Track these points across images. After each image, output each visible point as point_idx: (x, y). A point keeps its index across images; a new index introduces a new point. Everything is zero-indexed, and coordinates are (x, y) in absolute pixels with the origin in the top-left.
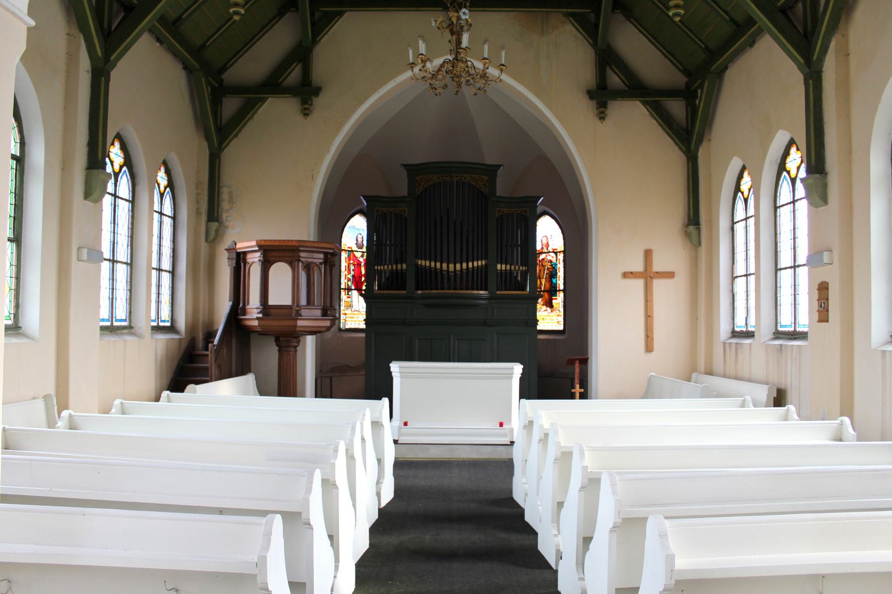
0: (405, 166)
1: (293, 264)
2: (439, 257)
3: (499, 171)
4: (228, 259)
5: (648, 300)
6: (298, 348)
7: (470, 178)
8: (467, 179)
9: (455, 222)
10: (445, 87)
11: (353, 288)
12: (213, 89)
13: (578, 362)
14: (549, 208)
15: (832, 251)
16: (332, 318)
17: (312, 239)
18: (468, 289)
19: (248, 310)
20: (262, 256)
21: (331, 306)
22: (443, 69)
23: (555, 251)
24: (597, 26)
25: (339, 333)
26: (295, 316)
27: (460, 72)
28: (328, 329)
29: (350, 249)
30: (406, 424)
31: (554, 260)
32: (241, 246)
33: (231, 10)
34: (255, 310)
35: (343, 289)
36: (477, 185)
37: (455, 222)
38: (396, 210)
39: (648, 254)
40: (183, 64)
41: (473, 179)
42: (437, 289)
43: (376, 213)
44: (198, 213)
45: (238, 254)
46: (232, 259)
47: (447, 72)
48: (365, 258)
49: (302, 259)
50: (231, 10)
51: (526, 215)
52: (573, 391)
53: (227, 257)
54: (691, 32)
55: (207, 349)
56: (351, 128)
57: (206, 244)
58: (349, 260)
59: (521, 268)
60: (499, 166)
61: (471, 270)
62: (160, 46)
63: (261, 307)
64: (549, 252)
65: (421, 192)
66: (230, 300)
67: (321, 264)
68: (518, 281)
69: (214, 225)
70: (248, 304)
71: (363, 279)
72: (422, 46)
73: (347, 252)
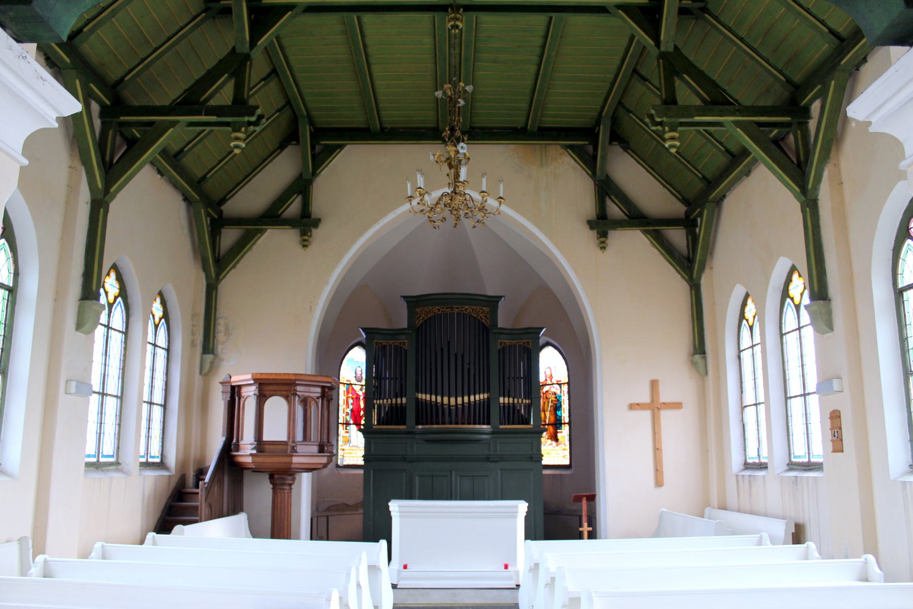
0: (404, 297)
3: (500, 302)
4: (223, 392)
5: (656, 432)
6: (293, 486)
7: (471, 310)
8: (468, 310)
9: (456, 355)
11: (352, 422)
12: (213, 220)
15: (841, 378)
16: (328, 454)
17: (309, 373)
18: (469, 424)
20: (257, 389)
21: (328, 442)
24: (595, 158)
25: (337, 470)
26: (290, 452)
28: (325, 466)
29: (349, 383)
30: (405, 567)
31: (558, 392)
32: (236, 379)
33: (232, 144)
34: (249, 446)
35: (341, 423)
37: (456, 355)
38: (395, 343)
39: (654, 384)
40: (183, 195)
41: (474, 310)
42: (438, 423)
44: (193, 344)
45: (233, 388)
47: (445, 206)
48: (364, 391)
49: (298, 393)
50: (232, 144)
51: (528, 346)
52: (581, 529)
53: (221, 390)
54: (688, 162)
57: (200, 376)
58: (348, 393)
59: (524, 401)
60: (501, 297)
63: (256, 443)
64: (553, 384)
65: (422, 324)
66: (223, 436)
67: (318, 398)
68: (522, 414)
69: (209, 357)
70: (242, 439)
71: (362, 413)
73: (346, 385)
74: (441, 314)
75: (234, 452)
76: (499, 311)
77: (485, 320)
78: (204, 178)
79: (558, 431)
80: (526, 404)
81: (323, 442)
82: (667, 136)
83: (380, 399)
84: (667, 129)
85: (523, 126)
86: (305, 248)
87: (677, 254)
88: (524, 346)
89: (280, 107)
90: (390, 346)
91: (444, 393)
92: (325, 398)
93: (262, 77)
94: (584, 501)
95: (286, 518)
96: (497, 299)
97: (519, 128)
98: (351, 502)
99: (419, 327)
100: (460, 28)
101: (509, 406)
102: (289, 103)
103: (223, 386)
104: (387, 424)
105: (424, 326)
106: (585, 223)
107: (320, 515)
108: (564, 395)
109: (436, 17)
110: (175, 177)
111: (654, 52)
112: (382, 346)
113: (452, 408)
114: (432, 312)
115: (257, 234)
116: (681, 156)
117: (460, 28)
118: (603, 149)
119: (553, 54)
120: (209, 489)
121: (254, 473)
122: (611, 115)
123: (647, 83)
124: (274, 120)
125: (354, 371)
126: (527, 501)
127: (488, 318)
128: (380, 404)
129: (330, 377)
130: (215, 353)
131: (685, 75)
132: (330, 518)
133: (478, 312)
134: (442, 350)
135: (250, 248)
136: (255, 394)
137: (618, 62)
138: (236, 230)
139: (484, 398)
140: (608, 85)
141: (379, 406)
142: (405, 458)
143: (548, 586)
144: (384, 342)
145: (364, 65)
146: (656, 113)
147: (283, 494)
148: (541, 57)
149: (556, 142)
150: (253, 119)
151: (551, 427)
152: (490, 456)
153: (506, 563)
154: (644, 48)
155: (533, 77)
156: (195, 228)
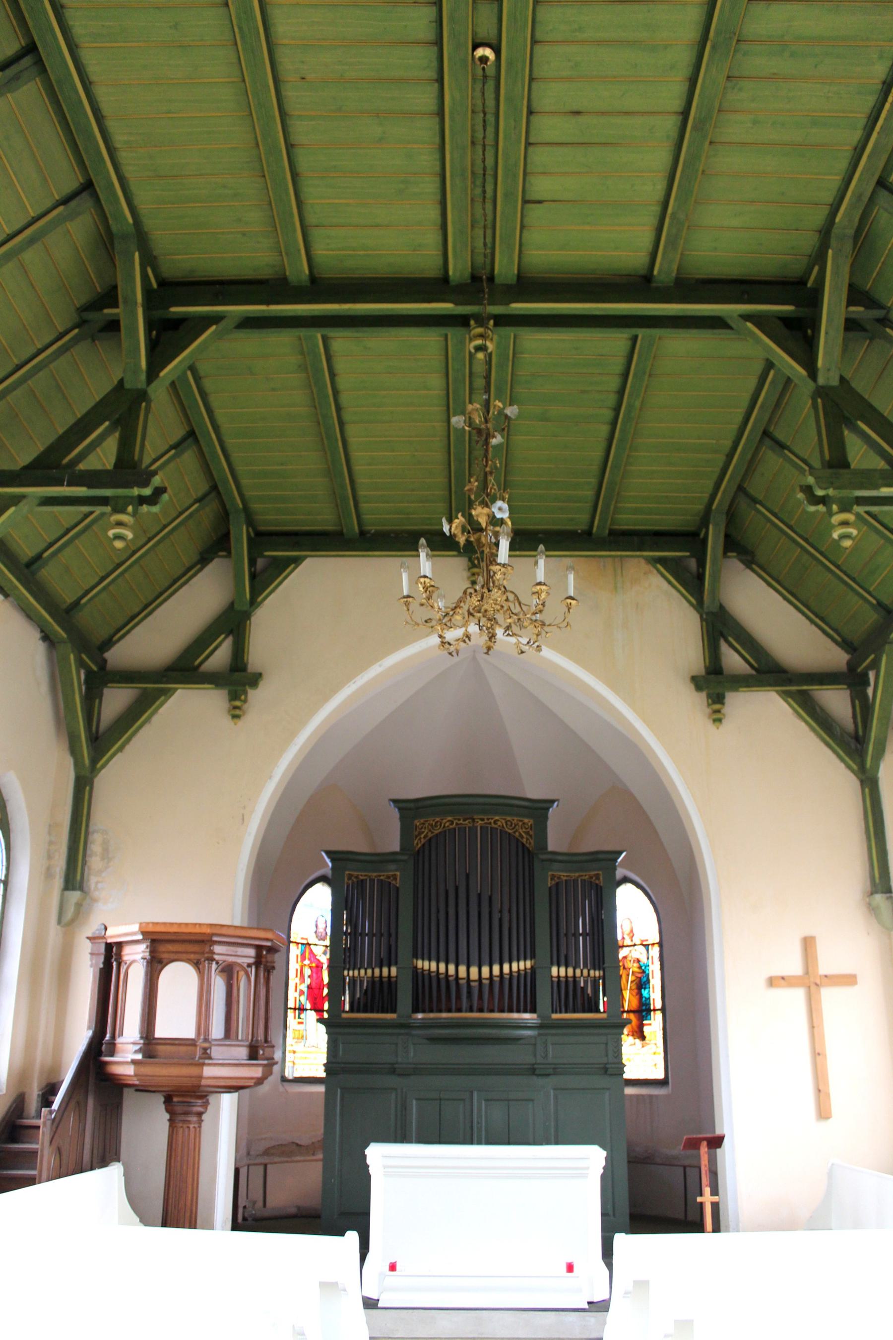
0: (395, 801)
1: (201, 967)
2: (452, 955)
3: (551, 810)
4: (92, 954)
5: (815, 1025)
6: (204, 1117)
7: (503, 821)
8: (499, 823)
9: (479, 895)
10: (467, 640)
11: (308, 1006)
12: (89, 674)
13: (705, 1143)
14: (631, 870)
16: (265, 1062)
17: (237, 923)
18: (502, 1011)
19: (119, 1046)
20: (148, 950)
21: (266, 1041)
22: (462, 604)
23: (644, 943)
24: (701, 577)
25: (283, 1085)
26: (200, 1058)
27: (494, 611)
28: (260, 1081)
29: (305, 942)
30: (393, 1267)
31: (644, 960)
32: (114, 933)
33: (111, 533)
34: (131, 1046)
35: (291, 1008)
36: (514, 832)
37: (479, 895)
38: (380, 876)
39: (808, 944)
40: (42, 631)
41: (509, 823)
42: (449, 1011)
43: (346, 879)
44: (49, 874)
45: (109, 947)
46: (98, 954)
47: (470, 614)
48: (328, 956)
49: (216, 957)
50: (111, 533)
51: (597, 882)
52: (699, 1199)
53: (89, 951)
54: (853, 580)
55: (39, 1116)
56: (309, 739)
57: (59, 927)
58: (303, 958)
59: (592, 972)
60: (553, 801)
61: (507, 977)
62: (3, 600)
63: (142, 1041)
64: (635, 945)
65: (423, 845)
66: (89, 1028)
67: (249, 965)
68: (588, 995)
69: (74, 896)
70: (121, 1034)
71: (326, 991)
72: (425, 567)
73: (300, 945)
74: (455, 829)
75: (106, 1056)
76: (550, 823)
77: (527, 839)
78: (76, 604)
79: (645, 1022)
80: (595, 977)
81: (257, 1040)
82: (836, 519)
83: (354, 970)
84: (835, 507)
85: (585, 527)
86: (236, 720)
87: (838, 729)
88: (591, 882)
89: (200, 493)
90: (372, 881)
91: (460, 960)
92: (262, 966)
93: (171, 443)
94: (704, 1148)
95: (190, 1172)
96: (544, 805)
97: (579, 531)
98: (305, 1141)
99: (418, 851)
100: (489, 351)
101: (567, 981)
102: (214, 488)
103: (92, 943)
104: (365, 1011)
105: (427, 847)
106: (688, 680)
107: (252, 1162)
108: (653, 963)
109: (449, 337)
110: (27, 599)
111: (806, 388)
112: (357, 882)
113: (473, 984)
114: (441, 825)
115: (160, 697)
116: (841, 570)
117: (489, 351)
118: (714, 563)
119: (637, 404)
120: (57, 1123)
121: (139, 1093)
122: (725, 507)
123: (786, 452)
124: (191, 516)
125: (314, 923)
126: (603, 1147)
127: (531, 836)
128: (353, 976)
129: (271, 930)
130: (86, 889)
131: (860, 423)
132: (269, 1167)
133: (515, 826)
134: (457, 888)
135: (148, 720)
136: (144, 958)
137: (739, 419)
138: (125, 690)
139: (526, 969)
140: (721, 458)
141: (353, 980)
142: (395, 1069)
143: (629, 1295)
144: (362, 875)
145: (334, 424)
146: (817, 483)
147: (187, 1130)
148: (617, 410)
149: (638, 553)
150: (147, 492)
151: (632, 1016)
152: (536, 1066)
153: (569, 1261)
154: (789, 380)
155: (603, 445)
156: (59, 687)
